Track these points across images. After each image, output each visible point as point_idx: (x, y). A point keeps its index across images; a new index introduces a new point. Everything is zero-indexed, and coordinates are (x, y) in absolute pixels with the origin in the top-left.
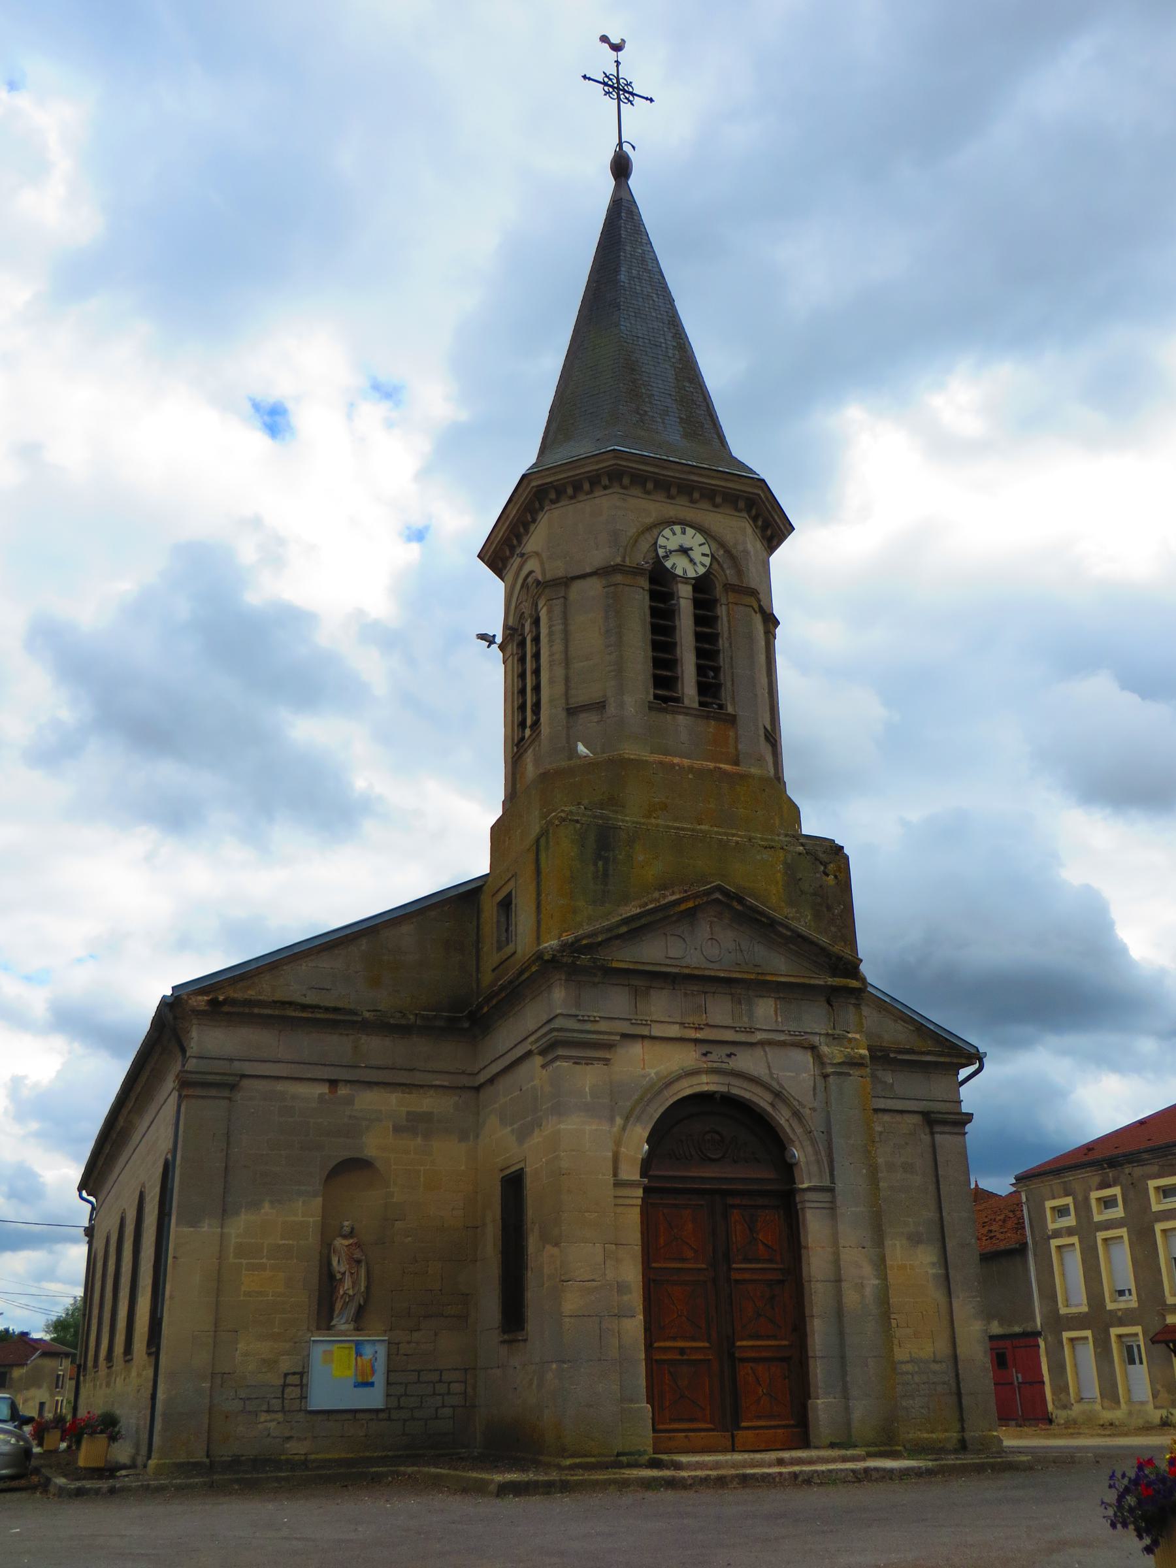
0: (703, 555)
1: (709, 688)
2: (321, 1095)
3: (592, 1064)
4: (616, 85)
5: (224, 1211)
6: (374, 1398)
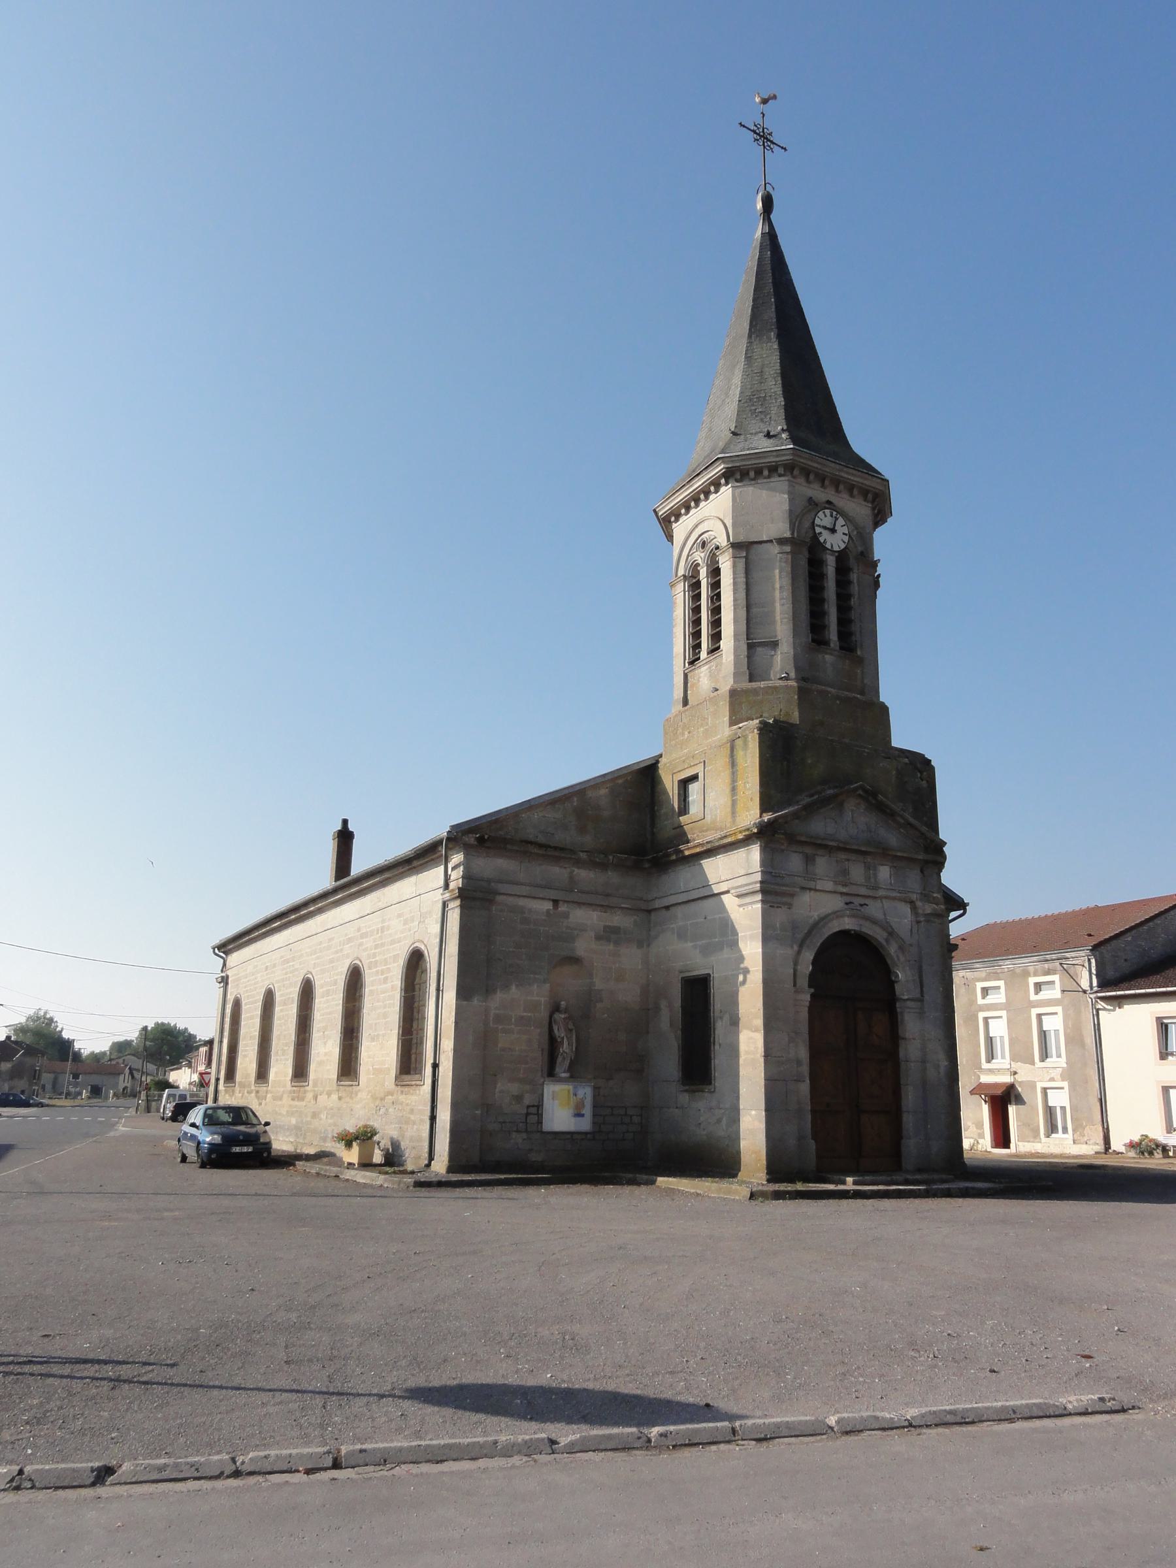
0: (844, 534)
1: (845, 635)
2: (548, 911)
3: (780, 907)
4: (762, 134)
5: (487, 990)
6: (585, 1125)
